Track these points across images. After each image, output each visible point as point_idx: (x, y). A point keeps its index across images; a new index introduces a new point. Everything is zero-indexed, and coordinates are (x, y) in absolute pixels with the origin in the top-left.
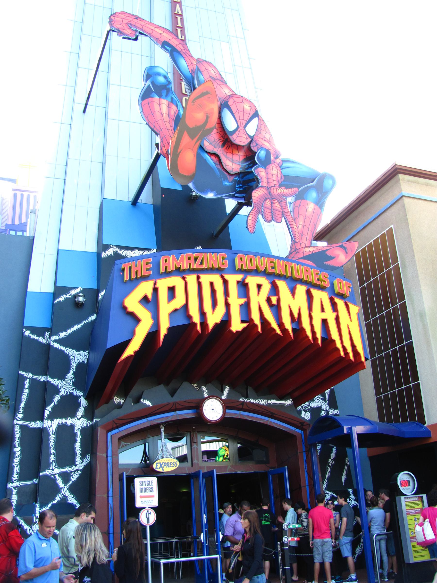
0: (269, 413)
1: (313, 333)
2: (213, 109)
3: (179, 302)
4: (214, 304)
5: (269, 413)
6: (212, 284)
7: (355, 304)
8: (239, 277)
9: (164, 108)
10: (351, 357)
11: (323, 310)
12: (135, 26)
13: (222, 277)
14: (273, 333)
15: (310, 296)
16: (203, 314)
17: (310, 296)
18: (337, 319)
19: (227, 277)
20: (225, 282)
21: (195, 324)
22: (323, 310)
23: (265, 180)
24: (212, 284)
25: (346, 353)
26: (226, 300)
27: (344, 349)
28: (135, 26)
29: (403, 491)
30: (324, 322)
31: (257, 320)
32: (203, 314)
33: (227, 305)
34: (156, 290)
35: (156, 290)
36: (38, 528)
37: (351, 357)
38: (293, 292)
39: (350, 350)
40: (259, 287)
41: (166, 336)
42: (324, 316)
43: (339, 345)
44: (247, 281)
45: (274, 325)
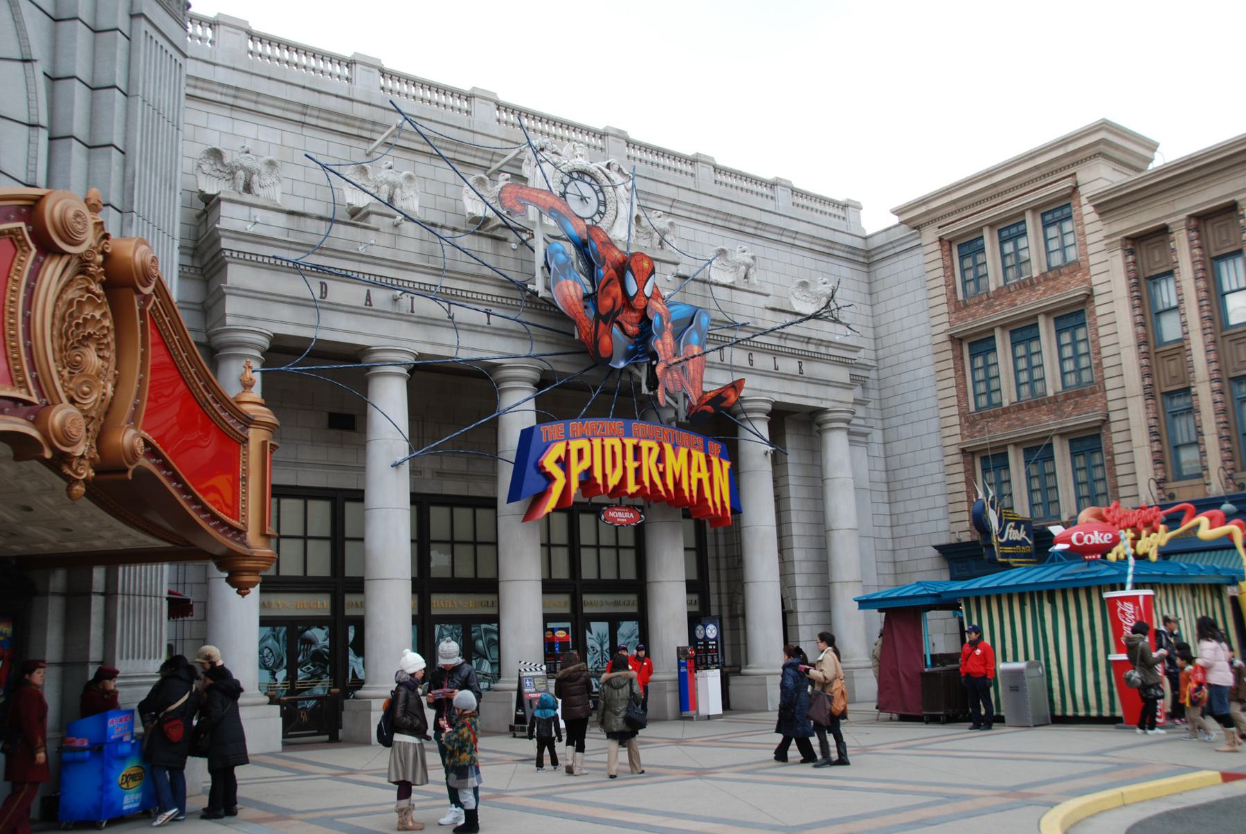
1: (691, 491)
2: (617, 293)
3: (586, 464)
6: (613, 447)
7: (726, 459)
8: (635, 441)
9: (572, 288)
11: (699, 470)
12: (523, 199)
13: (621, 440)
14: (658, 494)
15: (689, 455)
16: (605, 476)
17: (689, 455)
18: (711, 479)
19: (626, 441)
20: (624, 445)
21: (599, 485)
22: (699, 470)
24: (613, 447)
25: (716, 509)
26: (624, 463)
28: (523, 199)
30: (700, 481)
31: (647, 483)
32: (605, 476)
33: (625, 468)
34: (568, 452)
35: (568, 452)
36: (105, 352)
39: (695, 494)
40: (650, 449)
41: (575, 495)
42: (700, 475)
43: (710, 503)
44: (640, 445)
45: (661, 487)
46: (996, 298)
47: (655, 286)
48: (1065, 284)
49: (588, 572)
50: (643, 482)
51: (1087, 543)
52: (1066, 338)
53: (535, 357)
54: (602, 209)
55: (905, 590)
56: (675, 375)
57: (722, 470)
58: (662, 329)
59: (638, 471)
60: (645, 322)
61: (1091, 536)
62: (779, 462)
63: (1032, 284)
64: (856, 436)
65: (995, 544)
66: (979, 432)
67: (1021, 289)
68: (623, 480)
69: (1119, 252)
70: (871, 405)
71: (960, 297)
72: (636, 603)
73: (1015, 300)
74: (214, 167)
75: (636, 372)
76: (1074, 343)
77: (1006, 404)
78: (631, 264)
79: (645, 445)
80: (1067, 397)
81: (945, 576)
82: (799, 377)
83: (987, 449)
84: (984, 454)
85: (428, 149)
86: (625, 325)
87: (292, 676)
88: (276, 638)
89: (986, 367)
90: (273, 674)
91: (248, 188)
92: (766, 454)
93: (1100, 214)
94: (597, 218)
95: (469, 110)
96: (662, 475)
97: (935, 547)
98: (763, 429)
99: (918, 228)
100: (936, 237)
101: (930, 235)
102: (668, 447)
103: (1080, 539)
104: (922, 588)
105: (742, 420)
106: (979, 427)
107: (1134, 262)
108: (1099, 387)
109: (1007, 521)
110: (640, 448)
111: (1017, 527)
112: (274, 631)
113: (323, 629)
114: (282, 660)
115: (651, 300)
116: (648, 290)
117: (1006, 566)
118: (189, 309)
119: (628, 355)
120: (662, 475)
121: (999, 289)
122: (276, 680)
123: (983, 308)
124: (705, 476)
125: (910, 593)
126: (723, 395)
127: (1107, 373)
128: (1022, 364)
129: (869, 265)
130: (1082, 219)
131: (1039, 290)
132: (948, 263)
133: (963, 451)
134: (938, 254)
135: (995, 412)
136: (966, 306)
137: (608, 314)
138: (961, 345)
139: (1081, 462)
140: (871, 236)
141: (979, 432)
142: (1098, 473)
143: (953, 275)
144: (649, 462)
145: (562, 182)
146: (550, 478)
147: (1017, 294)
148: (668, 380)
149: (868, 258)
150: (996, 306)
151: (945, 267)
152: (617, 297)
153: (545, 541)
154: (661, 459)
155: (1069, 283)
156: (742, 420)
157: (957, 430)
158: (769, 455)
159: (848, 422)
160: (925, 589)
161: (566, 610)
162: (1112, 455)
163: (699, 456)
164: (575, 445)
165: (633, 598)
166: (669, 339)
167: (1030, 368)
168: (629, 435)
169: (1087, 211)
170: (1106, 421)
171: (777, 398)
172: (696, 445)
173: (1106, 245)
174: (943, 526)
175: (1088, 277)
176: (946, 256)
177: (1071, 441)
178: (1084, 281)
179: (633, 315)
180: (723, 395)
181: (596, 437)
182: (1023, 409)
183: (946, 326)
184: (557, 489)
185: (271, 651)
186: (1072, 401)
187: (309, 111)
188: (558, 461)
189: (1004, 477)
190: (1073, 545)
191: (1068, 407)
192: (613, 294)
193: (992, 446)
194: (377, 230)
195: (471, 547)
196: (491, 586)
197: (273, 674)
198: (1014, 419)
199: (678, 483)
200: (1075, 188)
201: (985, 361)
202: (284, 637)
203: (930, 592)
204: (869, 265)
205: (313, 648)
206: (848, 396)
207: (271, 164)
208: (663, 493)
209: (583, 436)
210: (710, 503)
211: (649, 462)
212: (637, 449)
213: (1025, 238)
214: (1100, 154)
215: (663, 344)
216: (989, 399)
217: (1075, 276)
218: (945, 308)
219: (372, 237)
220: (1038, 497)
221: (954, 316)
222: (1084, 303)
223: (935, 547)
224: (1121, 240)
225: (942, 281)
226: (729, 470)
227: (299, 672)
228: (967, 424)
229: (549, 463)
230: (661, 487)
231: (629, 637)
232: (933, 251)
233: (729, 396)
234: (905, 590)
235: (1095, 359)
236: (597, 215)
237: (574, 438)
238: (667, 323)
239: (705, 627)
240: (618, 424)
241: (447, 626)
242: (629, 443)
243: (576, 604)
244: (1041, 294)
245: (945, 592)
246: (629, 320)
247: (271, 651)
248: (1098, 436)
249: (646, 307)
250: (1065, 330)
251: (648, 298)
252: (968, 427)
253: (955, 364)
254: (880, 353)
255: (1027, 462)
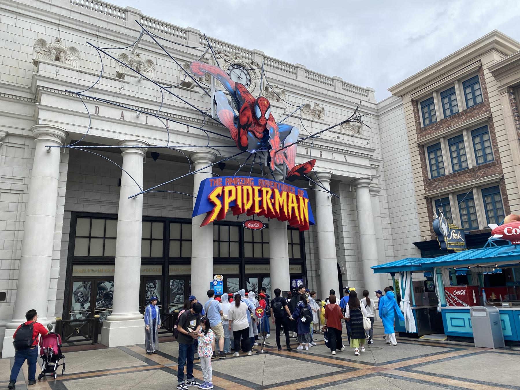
0: (421, 365)
1: (288, 213)
2: (249, 114)
3: (233, 198)
4: (248, 199)
5: (421, 365)
6: (248, 190)
7: (307, 198)
8: (259, 188)
10: (303, 223)
11: (293, 203)
13: (252, 187)
15: (288, 196)
16: (243, 204)
17: (288, 196)
18: (299, 207)
19: (254, 187)
20: (253, 190)
21: (240, 209)
22: (293, 203)
23: (274, 145)
24: (248, 190)
25: (301, 222)
27: (300, 219)
29: (299, 329)
30: (293, 208)
31: (265, 208)
32: (243, 204)
33: (254, 201)
34: (223, 192)
35: (223, 192)
37: (303, 223)
38: (281, 194)
39: (290, 214)
40: (267, 192)
41: (227, 213)
42: (293, 205)
43: (298, 219)
45: (272, 210)
46: (440, 125)
47: (270, 114)
48: (477, 114)
49: (248, 254)
50: (263, 208)
51: (515, 234)
52: (478, 140)
53: (210, 147)
54: (249, 83)
55: (398, 263)
56: (280, 156)
57: (304, 204)
58: (274, 135)
59: (261, 202)
60: (266, 132)
61: (517, 229)
62: (336, 203)
63: (459, 115)
64: (374, 192)
65: (446, 241)
66: (433, 188)
67: (453, 118)
68: (253, 206)
69: (506, 94)
70: (380, 178)
71: (422, 126)
72: (301, 269)
73: (450, 124)
74: (42, 49)
75: (262, 156)
76: (482, 142)
77: (447, 173)
78: (258, 102)
79: (264, 189)
80: (480, 168)
81: (420, 256)
82: (345, 163)
83: (439, 196)
84: (436, 199)
85: (164, 53)
86: (256, 133)
87: (92, 306)
88: (85, 287)
89: (436, 157)
90: (83, 305)
91: (57, 59)
92: (328, 197)
93: (495, 77)
94: (246, 87)
95: (186, 37)
96: (274, 205)
97: (414, 243)
98: (327, 186)
99: (401, 96)
100: (410, 100)
101: (408, 99)
102: (277, 191)
103: (510, 231)
104: (409, 261)
105: (317, 182)
106: (434, 186)
107: (515, 99)
108: (497, 162)
109: (451, 230)
110: (262, 191)
111: (456, 233)
112: (85, 283)
113: (111, 283)
114: (88, 298)
115: (268, 121)
116: (267, 116)
117: (452, 252)
118: (28, 120)
119: (258, 147)
120: (274, 205)
121: (441, 120)
122: (84, 308)
123: (434, 129)
124: (296, 205)
125: (402, 265)
126: (304, 167)
127: (501, 155)
128: (455, 155)
129: (378, 116)
130: (485, 81)
131: (462, 118)
132: (416, 111)
133: (426, 198)
134: (411, 107)
135: (441, 178)
136: (426, 130)
137: (245, 125)
138: (423, 148)
139: (489, 200)
140: (379, 103)
141: (433, 188)
142: (498, 206)
143: (419, 116)
144: (267, 198)
145: (229, 69)
146: (214, 205)
147: (451, 122)
148: (279, 159)
149: (378, 113)
150: (441, 128)
151: (414, 113)
152: (249, 117)
153: (217, 239)
154: (273, 196)
155: (479, 113)
156: (317, 182)
157: (423, 187)
158: (330, 198)
159: (369, 184)
160: (410, 262)
161: (237, 272)
162: (506, 195)
163: (292, 196)
164: (227, 189)
165: (299, 267)
166: (278, 139)
167: (459, 156)
168: (257, 185)
169: (488, 75)
170: (502, 179)
171: (335, 173)
172: (292, 191)
173: (498, 91)
174: (418, 233)
175: (489, 109)
176: (415, 108)
177: (483, 190)
178: (487, 111)
179: (260, 128)
180: (304, 167)
181: (239, 185)
182: (456, 176)
183: (416, 139)
184: (217, 210)
185: (82, 294)
186: (483, 170)
187: (100, 30)
188: (218, 196)
189: (447, 209)
190: (505, 235)
191: (481, 173)
192: (247, 115)
193: (441, 194)
194: (129, 83)
195: (179, 242)
196: (266, 261)
197: (83, 305)
198: (452, 181)
199: (281, 209)
200: (481, 67)
201: (436, 155)
202: (89, 287)
203: (413, 264)
204: (378, 116)
205: (105, 292)
206: (369, 172)
207: (73, 49)
208: (274, 213)
209: (232, 185)
210: (298, 219)
211: (267, 198)
212: (260, 192)
213: (454, 95)
214: (494, 49)
215: (274, 142)
216: (438, 173)
217: (482, 109)
218: (415, 132)
219: (127, 86)
220: (465, 219)
221: (420, 135)
222: (487, 121)
223: (414, 243)
224: (507, 87)
225: (413, 119)
226: (308, 203)
227: (97, 304)
228: (427, 185)
229: (213, 197)
230: (272, 210)
231: (267, 285)
232: (409, 106)
233: (308, 168)
234: (398, 263)
235: (494, 148)
236: (246, 86)
237: (227, 185)
238: (277, 132)
239: (296, 282)
240: (250, 179)
241: (177, 280)
242: (256, 188)
243: (242, 269)
244: (464, 120)
245: (424, 264)
246: (258, 130)
247: (82, 294)
248: (498, 187)
249: (266, 124)
250: (477, 136)
251: (267, 120)
252: (428, 186)
253: (421, 157)
254: (384, 156)
255: (459, 202)
